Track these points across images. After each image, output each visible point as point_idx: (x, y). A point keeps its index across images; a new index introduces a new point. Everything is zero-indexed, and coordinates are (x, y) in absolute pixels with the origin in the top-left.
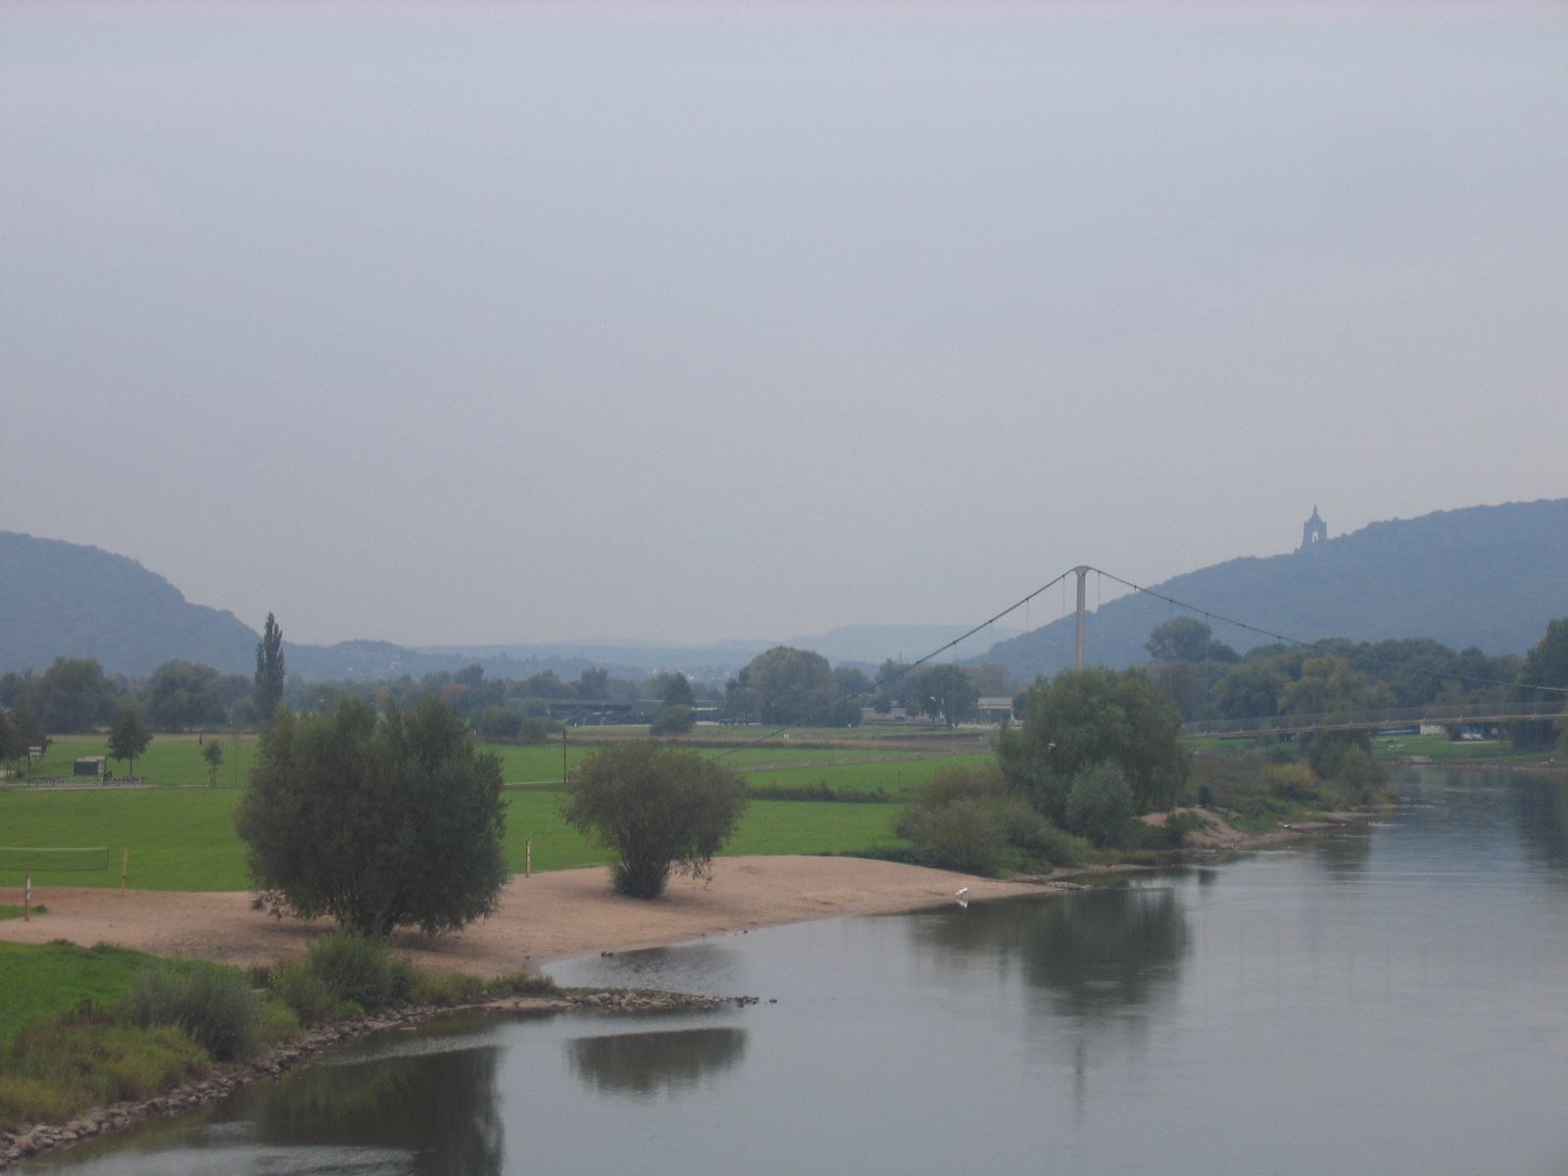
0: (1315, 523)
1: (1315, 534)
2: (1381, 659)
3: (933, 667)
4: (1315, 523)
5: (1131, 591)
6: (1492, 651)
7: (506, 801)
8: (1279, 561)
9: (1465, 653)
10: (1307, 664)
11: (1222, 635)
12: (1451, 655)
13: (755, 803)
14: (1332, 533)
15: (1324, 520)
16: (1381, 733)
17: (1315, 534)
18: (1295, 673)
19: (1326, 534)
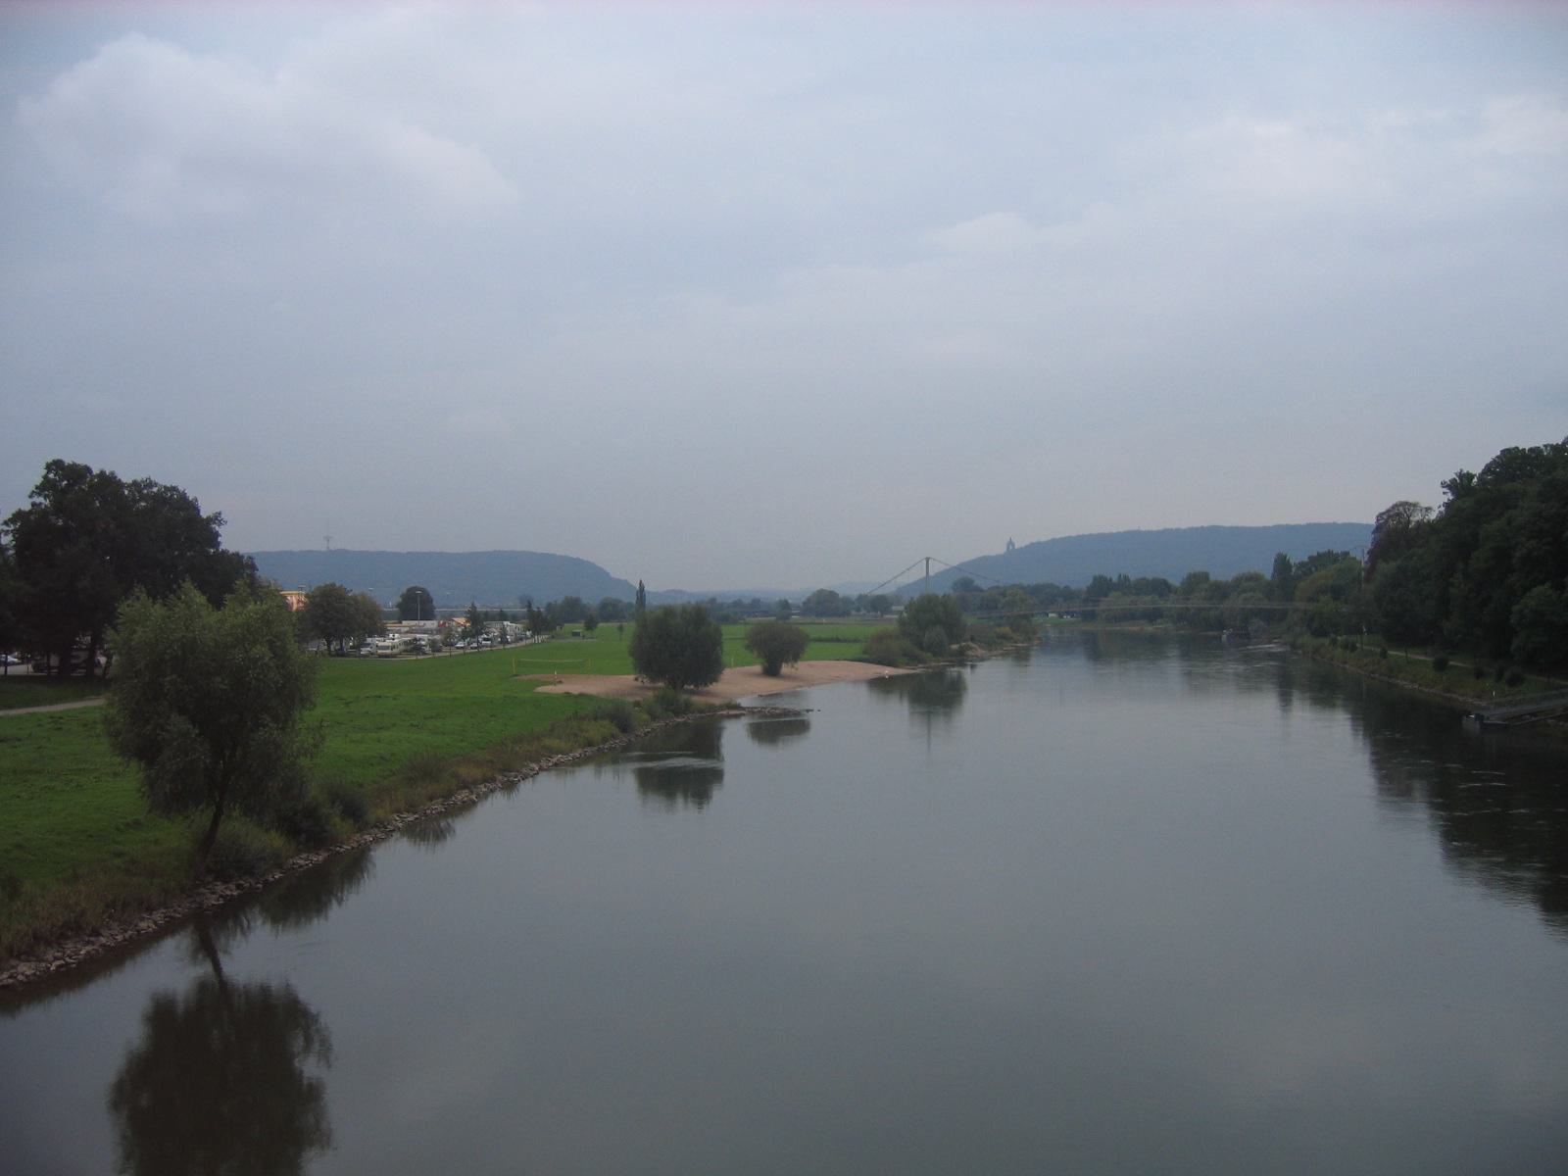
0: (1011, 543)
2: (1034, 590)
4: (1011, 543)
6: (1074, 587)
11: (979, 582)
12: (1058, 588)
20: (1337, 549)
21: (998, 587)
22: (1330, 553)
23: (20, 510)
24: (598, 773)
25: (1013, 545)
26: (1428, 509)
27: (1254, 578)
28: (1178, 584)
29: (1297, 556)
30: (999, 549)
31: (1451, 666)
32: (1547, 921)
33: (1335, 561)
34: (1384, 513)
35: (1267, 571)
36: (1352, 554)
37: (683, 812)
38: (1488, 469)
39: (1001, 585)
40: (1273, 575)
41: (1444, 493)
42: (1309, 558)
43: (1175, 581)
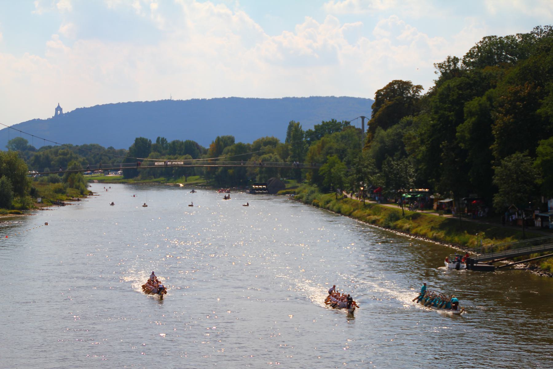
0: (59, 108)
1: (59, 112)
2: (84, 150)
3: (273, 195)
4: (59, 108)
5: (6, 127)
6: (117, 148)
7: (434, 82)
8: (49, 120)
9: (109, 148)
10: (60, 151)
11: (31, 143)
12: (104, 149)
13: (50, 174)
14: (64, 112)
15: (61, 107)
16: (94, 194)
17: (59, 112)
18: (56, 153)
19: (62, 112)
20: (340, 119)
21: (50, 147)
22: (333, 122)
23: (218, 138)
24: (267, 137)
25: (61, 110)
26: (419, 87)
27: (273, 143)
28: (207, 147)
29: (307, 126)
30: (47, 114)
31: (348, 183)
32: (311, 210)
33: (338, 130)
34: (381, 90)
35: (282, 138)
36: (352, 124)
37: (517, 33)
38: (470, 55)
39: (53, 145)
40: (287, 140)
41: (436, 72)
42: (315, 127)
43: (206, 143)
